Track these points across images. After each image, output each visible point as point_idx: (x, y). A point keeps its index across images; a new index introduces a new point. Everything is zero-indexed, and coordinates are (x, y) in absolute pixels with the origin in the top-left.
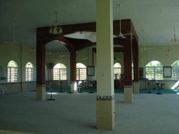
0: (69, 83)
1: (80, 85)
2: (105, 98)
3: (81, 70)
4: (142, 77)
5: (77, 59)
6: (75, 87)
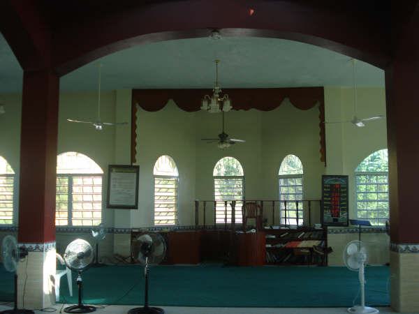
0: (6, 254)
1: (76, 262)
2: (123, 230)
3: (76, 181)
4: (342, 216)
5: (67, 120)
6: (48, 270)
